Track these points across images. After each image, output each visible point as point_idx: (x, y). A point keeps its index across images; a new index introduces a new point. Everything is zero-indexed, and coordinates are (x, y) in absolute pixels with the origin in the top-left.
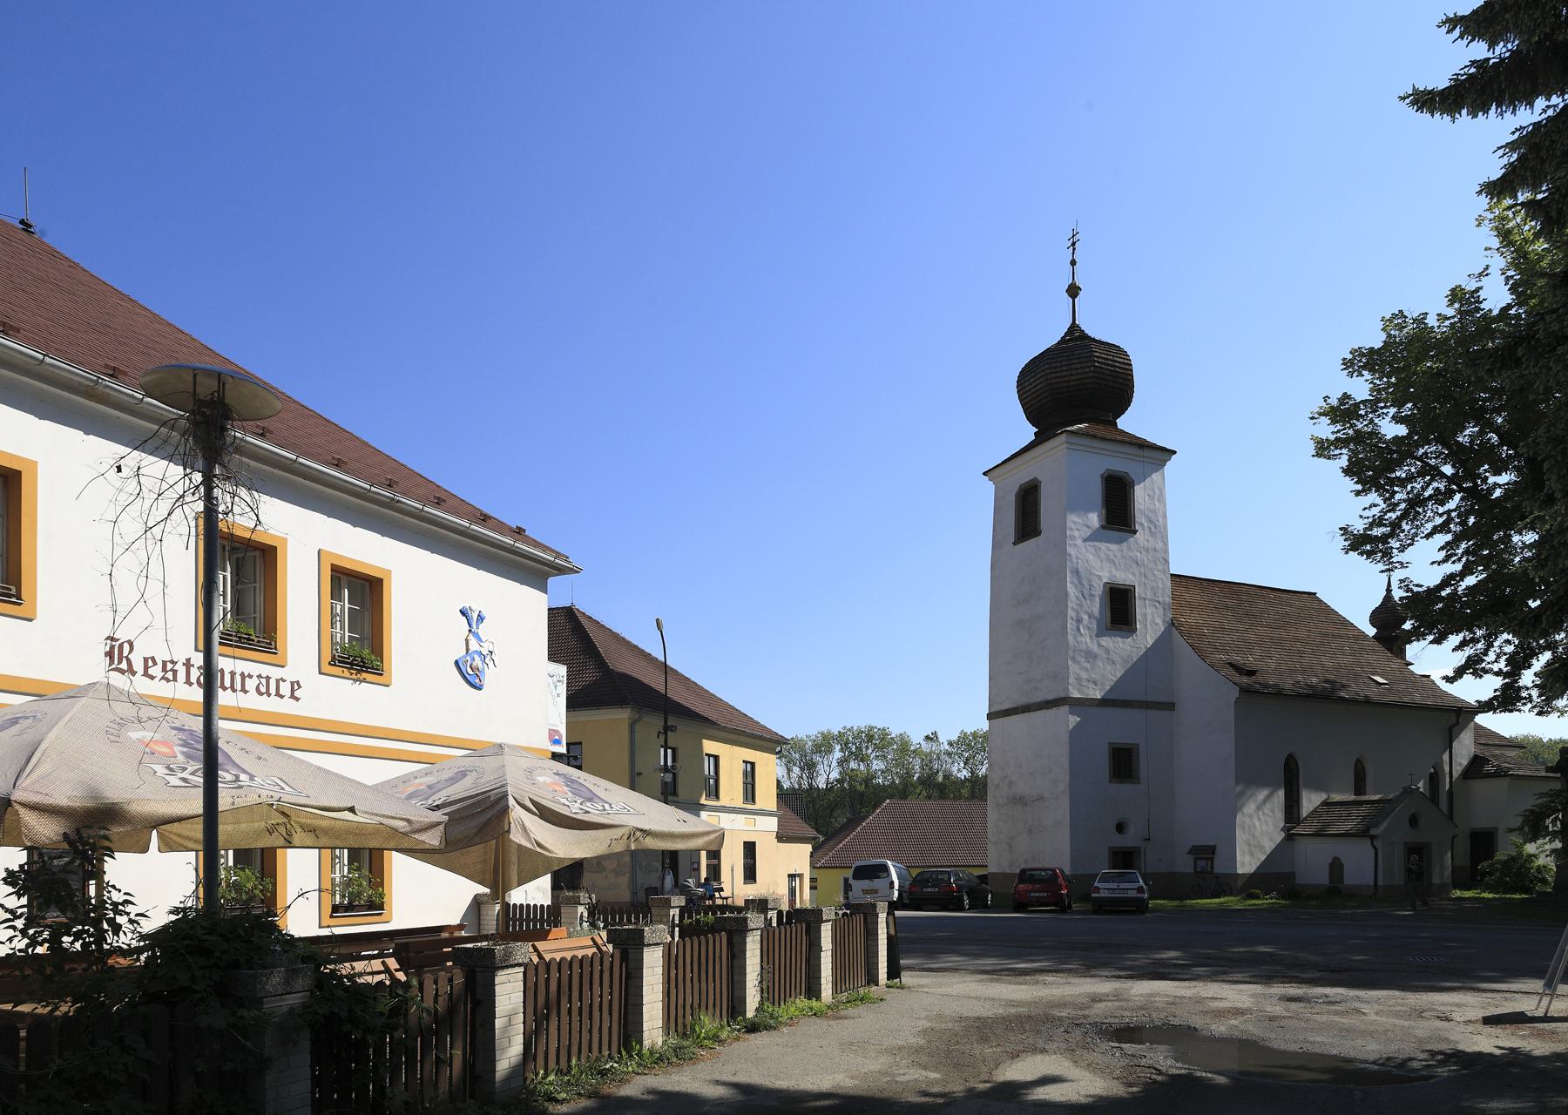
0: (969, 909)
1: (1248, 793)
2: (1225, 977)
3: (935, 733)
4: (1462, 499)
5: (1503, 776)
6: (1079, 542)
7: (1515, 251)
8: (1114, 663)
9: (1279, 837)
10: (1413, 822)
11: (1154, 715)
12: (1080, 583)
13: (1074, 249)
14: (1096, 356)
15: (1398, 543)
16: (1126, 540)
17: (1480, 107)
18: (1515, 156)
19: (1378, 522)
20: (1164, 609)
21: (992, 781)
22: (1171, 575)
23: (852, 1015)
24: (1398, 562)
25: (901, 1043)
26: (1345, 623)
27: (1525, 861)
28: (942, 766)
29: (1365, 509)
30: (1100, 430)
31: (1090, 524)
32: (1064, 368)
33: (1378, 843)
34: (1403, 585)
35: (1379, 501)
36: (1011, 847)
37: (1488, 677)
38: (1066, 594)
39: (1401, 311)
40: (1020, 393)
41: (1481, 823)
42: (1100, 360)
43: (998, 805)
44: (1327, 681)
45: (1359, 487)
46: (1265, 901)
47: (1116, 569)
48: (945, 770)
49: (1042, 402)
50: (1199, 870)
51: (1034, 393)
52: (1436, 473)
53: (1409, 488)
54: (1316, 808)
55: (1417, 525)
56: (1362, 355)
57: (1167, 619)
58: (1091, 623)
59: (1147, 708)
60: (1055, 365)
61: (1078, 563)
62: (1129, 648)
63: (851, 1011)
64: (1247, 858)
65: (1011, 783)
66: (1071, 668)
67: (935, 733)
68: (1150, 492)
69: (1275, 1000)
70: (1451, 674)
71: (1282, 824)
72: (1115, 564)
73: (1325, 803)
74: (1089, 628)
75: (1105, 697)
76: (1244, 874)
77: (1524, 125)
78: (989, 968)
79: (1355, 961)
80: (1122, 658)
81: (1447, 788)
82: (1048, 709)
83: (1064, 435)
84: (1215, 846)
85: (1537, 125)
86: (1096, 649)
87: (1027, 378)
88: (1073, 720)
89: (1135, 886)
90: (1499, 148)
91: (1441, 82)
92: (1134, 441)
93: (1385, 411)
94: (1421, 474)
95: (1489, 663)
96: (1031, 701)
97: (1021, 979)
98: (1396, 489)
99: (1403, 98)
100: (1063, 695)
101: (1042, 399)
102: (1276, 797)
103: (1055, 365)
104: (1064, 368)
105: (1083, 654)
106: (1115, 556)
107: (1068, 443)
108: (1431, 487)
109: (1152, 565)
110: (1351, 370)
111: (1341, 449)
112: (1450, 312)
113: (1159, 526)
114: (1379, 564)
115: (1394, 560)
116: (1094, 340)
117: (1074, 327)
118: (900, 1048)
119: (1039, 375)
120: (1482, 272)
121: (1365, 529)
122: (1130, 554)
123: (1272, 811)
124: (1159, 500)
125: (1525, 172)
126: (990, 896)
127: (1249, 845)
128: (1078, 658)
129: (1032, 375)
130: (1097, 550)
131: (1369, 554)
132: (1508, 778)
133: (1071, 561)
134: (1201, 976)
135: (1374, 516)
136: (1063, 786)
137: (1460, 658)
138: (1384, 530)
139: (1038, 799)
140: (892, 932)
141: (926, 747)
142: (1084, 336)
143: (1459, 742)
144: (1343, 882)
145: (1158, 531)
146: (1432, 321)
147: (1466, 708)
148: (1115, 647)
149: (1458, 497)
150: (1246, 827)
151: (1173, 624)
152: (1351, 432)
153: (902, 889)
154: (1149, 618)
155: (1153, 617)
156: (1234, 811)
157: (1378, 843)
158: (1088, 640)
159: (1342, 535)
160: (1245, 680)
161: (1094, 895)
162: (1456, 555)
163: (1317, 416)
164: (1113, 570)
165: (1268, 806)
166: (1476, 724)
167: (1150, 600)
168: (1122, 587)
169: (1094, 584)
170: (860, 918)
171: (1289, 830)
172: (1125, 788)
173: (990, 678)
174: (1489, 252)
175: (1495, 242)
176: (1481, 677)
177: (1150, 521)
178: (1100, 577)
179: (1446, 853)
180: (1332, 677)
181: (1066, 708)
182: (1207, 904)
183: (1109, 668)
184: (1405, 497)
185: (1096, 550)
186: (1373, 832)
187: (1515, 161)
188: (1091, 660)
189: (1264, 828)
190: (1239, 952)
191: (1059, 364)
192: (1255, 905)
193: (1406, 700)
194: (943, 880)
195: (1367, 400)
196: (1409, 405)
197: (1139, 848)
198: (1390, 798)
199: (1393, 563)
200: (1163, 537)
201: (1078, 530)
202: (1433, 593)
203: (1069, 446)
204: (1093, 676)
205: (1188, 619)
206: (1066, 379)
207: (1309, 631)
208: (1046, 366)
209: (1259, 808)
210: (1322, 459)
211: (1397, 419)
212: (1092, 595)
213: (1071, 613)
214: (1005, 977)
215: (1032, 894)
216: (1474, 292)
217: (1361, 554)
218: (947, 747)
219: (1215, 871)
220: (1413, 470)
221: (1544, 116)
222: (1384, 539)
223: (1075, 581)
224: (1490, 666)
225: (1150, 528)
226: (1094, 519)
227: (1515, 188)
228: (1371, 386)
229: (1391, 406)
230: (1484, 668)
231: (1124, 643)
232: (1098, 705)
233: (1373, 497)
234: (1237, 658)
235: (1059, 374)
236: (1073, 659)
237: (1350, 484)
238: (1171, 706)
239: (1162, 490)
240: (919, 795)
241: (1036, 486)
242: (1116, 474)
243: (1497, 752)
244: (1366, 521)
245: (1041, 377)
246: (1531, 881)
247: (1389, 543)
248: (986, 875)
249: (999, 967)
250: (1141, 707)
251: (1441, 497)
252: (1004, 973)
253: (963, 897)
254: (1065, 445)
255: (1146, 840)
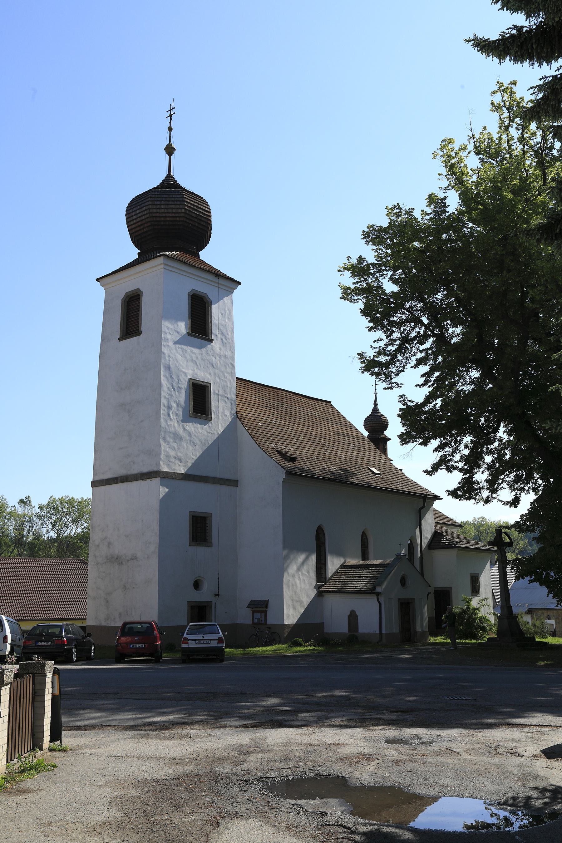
0: (76, 661)
1: (292, 557)
2: (327, 722)
3: (28, 498)
4: (434, 342)
5: (452, 548)
6: (171, 344)
7: (456, 179)
8: (194, 444)
9: (313, 593)
10: (403, 581)
11: (224, 489)
12: (171, 377)
13: (171, 119)
14: (187, 202)
15: (395, 369)
16: (205, 346)
17: (519, 57)
18: (540, 95)
19: (382, 352)
20: (231, 403)
21: (94, 541)
22: (237, 378)
23: (32, 787)
24: (395, 383)
25: (99, 818)
26: (350, 426)
27: (472, 613)
28: (33, 527)
29: (375, 341)
30: (188, 258)
31: (179, 331)
32: (162, 206)
33: (382, 599)
34: (401, 399)
35: (383, 336)
36: (107, 602)
37: (456, 472)
38: (160, 385)
39: (398, 204)
40: (128, 220)
41: (441, 583)
42: (189, 205)
43: (98, 564)
44: (342, 469)
45: (371, 325)
46: (306, 648)
47: (198, 368)
48: (35, 531)
49: (145, 230)
50: (256, 621)
51: (139, 222)
52: (419, 322)
53: (402, 330)
54: (337, 570)
55: (407, 357)
56: (374, 230)
57: (234, 412)
58: (178, 410)
59: (218, 483)
60: (156, 203)
61: (169, 360)
62: (206, 433)
63: (28, 783)
64: (291, 612)
65: (109, 544)
66: (162, 447)
67: (28, 498)
68: (223, 312)
69: (382, 742)
70: (430, 469)
71: (314, 583)
72: (196, 364)
73: (343, 566)
74: (177, 415)
75: (188, 473)
76: (289, 625)
77: (547, 76)
78: (132, 723)
79: (410, 701)
80: (200, 441)
81: (419, 556)
82: (143, 480)
83: (162, 258)
84: (268, 600)
85: (554, 77)
86: (181, 432)
87: (134, 209)
88: (163, 491)
89: (216, 636)
90: (531, 88)
91: (494, 36)
92: (212, 270)
93: (385, 273)
94: (408, 321)
95: (456, 462)
96: (129, 473)
97: (166, 733)
98: (394, 329)
99: (469, 41)
100: (155, 469)
101: (145, 227)
102: (310, 560)
103: (156, 203)
104: (162, 206)
105: (172, 435)
106: (197, 358)
107: (165, 264)
108: (414, 332)
109: (223, 369)
110: (367, 239)
111: (358, 295)
112: (429, 210)
113: (229, 338)
114: (384, 382)
115: (393, 381)
116: (184, 189)
117: (169, 177)
118: (101, 825)
119: (144, 209)
120: (447, 187)
121: (374, 356)
122: (208, 357)
123: (308, 572)
124: (229, 319)
125: (548, 107)
126: (93, 648)
127: (292, 600)
128: (168, 439)
129: (138, 207)
130: (185, 351)
131: (378, 375)
132: (456, 549)
133: (165, 358)
134: (310, 721)
135: (380, 347)
136: (154, 547)
137: (435, 457)
138: (387, 358)
139: (132, 559)
140: (57, 692)
141: (20, 510)
142: (176, 185)
143: (426, 521)
144: (357, 631)
145: (228, 343)
146: (417, 214)
147: (429, 495)
148: (196, 432)
149: (431, 340)
150: (291, 585)
151: (237, 416)
152: (364, 284)
153: (14, 643)
154: (221, 410)
155: (224, 410)
156: (282, 570)
157: (382, 599)
158: (176, 424)
159: (359, 359)
160: (289, 465)
161: (184, 646)
162: (431, 381)
163: (342, 270)
164: (196, 370)
165: (305, 567)
166: (435, 511)
167: (222, 396)
168: (202, 383)
169: (182, 380)
170: (28, 679)
171: (319, 588)
172: (201, 551)
173: (96, 451)
174: (440, 177)
175: (444, 171)
176: (451, 472)
177: (222, 334)
178: (185, 374)
179: (424, 608)
180: (344, 467)
181: (157, 480)
182: (265, 651)
183: (191, 448)
184: (399, 335)
185: (183, 352)
186: (379, 589)
187: (540, 99)
188: (177, 441)
189: (303, 586)
190: (323, 697)
191: (159, 203)
192: (300, 651)
193: (393, 487)
194: (54, 633)
195: (374, 263)
196: (400, 271)
197: (211, 602)
198: (387, 562)
199: (391, 383)
200: (231, 347)
201: (171, 334)
202: (419, 407)
203: (166, 267)
204: (179, 454)
205: (249, 413)
206: (164, 215)
207: (328, 430)
208: (149, 203)
209: (299, 569)
210: (346, 302)
211: (393, 280)
212: (179, 388)
213: (163, 401)
214: (151, 733)
215: (133, 646)
216: (442, 199)
217: (372, 374)
218: (38, 510)
219: (268, 623)
220: (404, 317)
221: (557, 73)
222: (387, 365)
223: (167, 375)
224: (456, 464)
225: (222, 339)
226: (183, 327)
227: (540, 117)
228: (376, 254)
229: (389, 270)
230: (453, 465)
231: (202, 429)
232: (182, 479)
233: (379, 333)
234: (282, 448)
235: (158, 211)
236: (164, 439)
237: (366, 322)
238: (235, 483)
239: (230, 311)
240: (12, 552)
241: (139, 295)
242: (199, 293)
243: (447, 529)
244: (375, 350)
245: (146, 210)
246: (476, 629)
247: (390, 368)
248: (85, 627)
249: (140, 722)
250: (213, 483)
251: (422, 339)
252: (147, 728)
253: (72, 649)
254: (162, 266)
255: (216, 595)
